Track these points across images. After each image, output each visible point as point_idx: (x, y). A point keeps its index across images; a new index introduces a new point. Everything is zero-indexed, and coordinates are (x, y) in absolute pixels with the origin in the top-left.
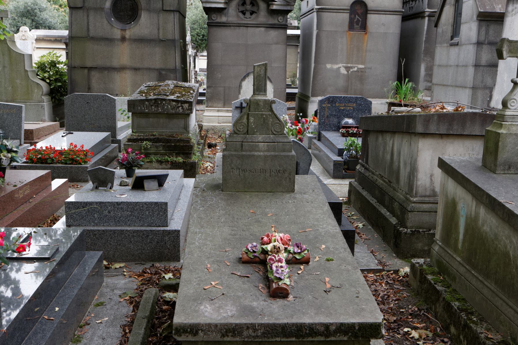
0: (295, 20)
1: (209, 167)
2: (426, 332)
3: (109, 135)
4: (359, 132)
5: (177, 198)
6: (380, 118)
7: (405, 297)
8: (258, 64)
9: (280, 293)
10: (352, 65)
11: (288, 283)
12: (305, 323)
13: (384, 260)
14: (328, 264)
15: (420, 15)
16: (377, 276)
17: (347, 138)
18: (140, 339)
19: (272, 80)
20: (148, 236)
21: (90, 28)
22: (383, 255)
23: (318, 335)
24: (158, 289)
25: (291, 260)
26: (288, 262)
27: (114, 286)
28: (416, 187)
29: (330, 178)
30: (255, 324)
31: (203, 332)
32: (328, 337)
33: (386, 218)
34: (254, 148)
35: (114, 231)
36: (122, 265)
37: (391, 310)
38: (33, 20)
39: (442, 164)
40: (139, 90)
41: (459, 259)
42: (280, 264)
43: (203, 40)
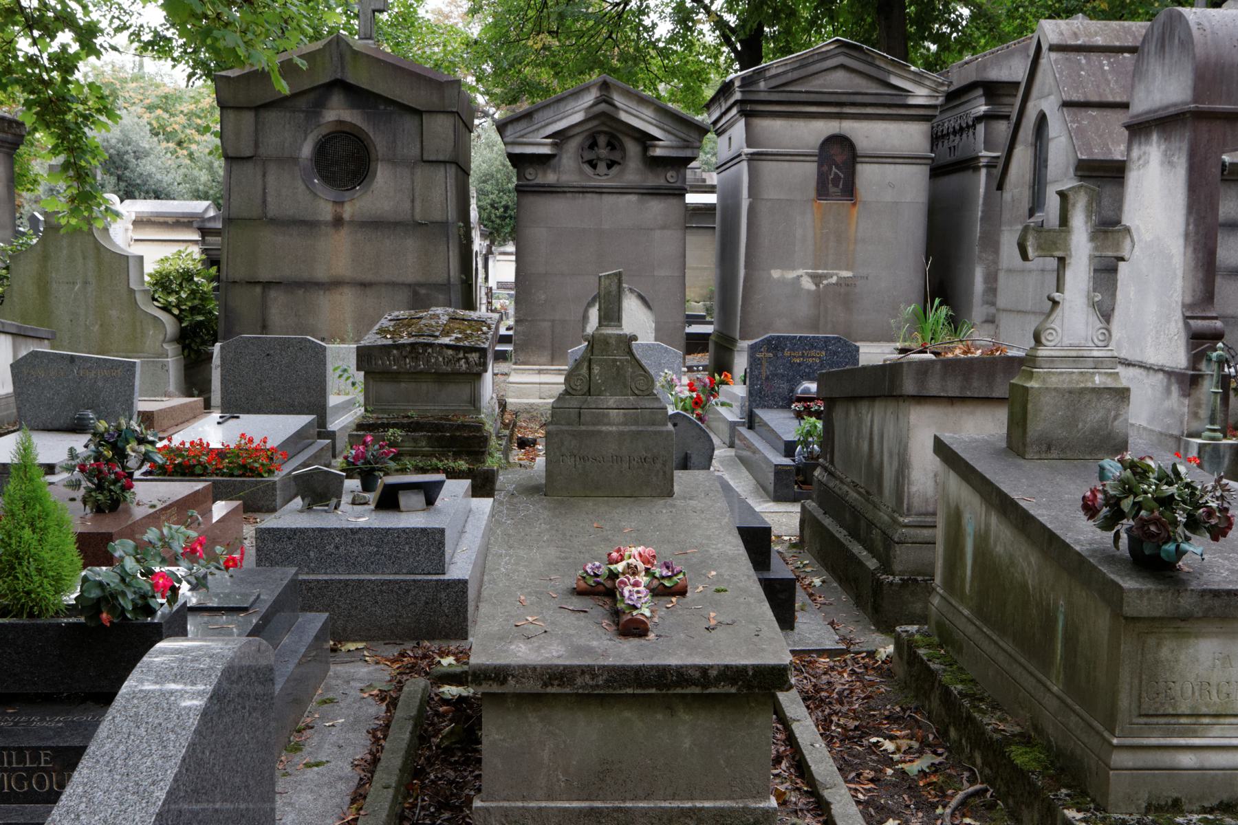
2: (909, 742)
7: (882, 693)
14: (717, 596)
15: (968, 164)
20: (408, 591)
21: (269, 199)
22: (850, 629)
28: (909, 496)
29: (767, 502)
34: (600, 419)
36: (360, 645)
38: (119, 178)
39: (941, 448)
40: (377, 327)
41: (966, 612)
43: (506, 218)
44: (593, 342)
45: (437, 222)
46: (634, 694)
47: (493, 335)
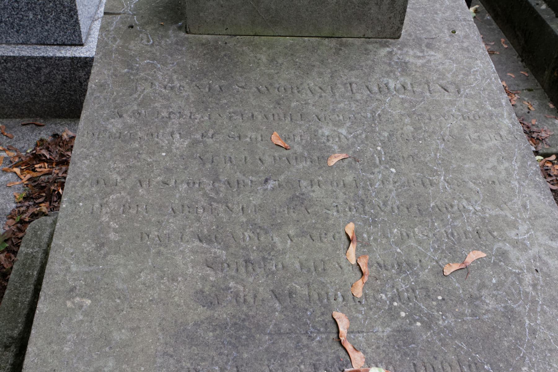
20: (39, 69)
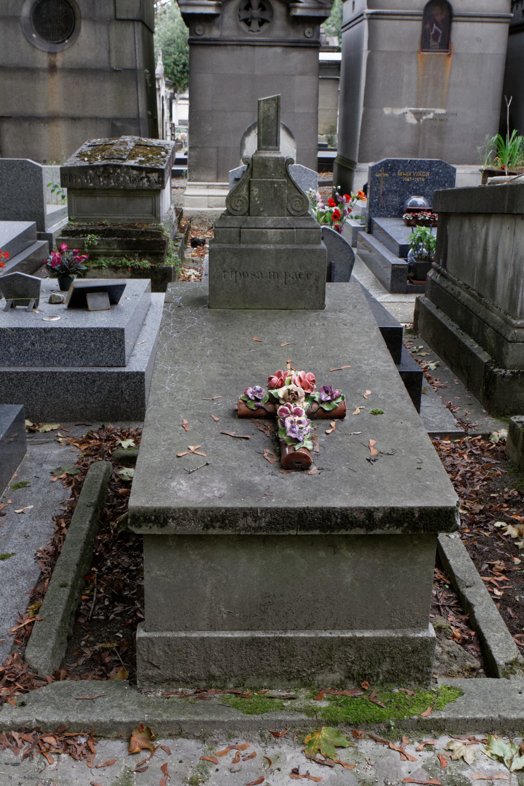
0: (334, 36)
1: (193, 277)
3: (33, 225)
4: (434, 219)
5: (140, 323)
6: (468, 191)
8: (266, 98)
9: (297, 463)
10: (425, 109)
11: (310, 447)
12: (334, 508)
13: (468, 419)
14: (375, 419)
16: (455, 443)
17: (414, 229)
18: (83, 536)
19: (294, 134)
20: (94, 381)
23: (355, 525)
24: (111, 463)
25: (316, 412)
26: (311, 416)
27: (42, 459)
29: (385, 293)
30: (257, 509)
31: (175, 521)
32: (371, 530)
33: (472, 352)
34: (259, 238)
35: (41, 374)
36: (55, 426)
37: (477, 495)
42: (297, 418)
44: (251, 164)
45: (128, 69)
46: (297, 535)
47: (170, 159)
